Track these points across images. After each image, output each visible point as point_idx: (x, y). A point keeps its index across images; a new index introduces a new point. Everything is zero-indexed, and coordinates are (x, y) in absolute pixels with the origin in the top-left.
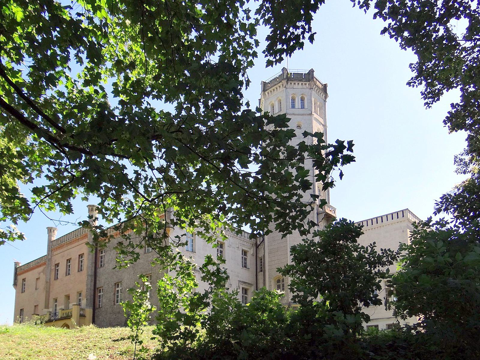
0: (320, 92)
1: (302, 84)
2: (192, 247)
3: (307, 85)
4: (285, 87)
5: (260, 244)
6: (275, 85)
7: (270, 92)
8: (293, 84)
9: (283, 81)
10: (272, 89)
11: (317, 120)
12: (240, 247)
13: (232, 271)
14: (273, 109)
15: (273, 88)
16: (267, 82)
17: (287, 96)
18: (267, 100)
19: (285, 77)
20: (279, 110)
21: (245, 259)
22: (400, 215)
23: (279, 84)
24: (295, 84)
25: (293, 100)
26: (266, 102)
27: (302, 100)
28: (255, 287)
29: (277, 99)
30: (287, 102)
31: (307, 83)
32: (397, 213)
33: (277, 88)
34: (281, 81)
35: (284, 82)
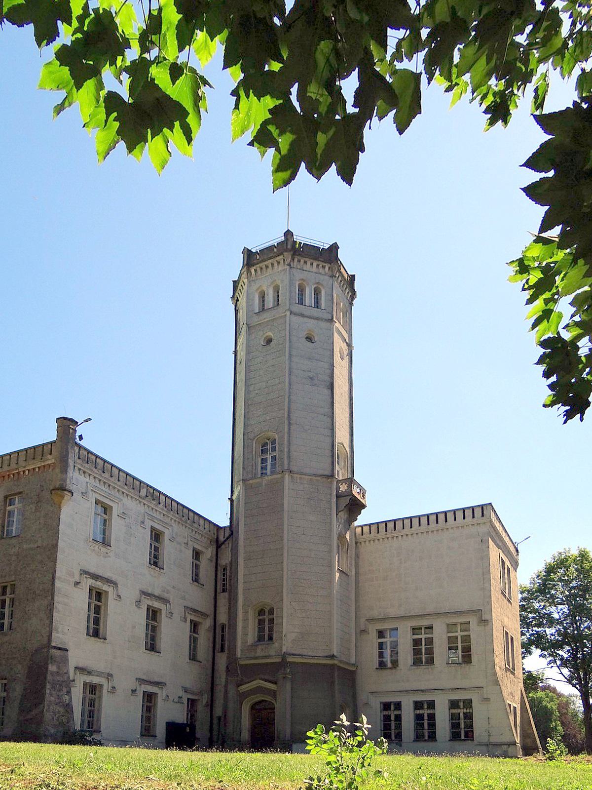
0: (345, 286)
1: (318, 265)
2: (104, 534)
3: (327, 269)
4: (289, 265)
5: (225, 541)
6: (271, 258)
7: (258, 269)
8: (302, 261)
9: (285, 254)
10: (263, 265)
11: (340, 333)
12: (190, 543)
13: (174, 587)
14: (263, 301)
15: (266, 263)
16: (254, 251)
17: (291, 281)
18: (253, 284)
19: (289, 247)
20: (274, 304)
21: (197, 567)
22: (478, 512)
23: (278, 259)
24: (305, 262)
25: (302, 290)
26: (249, 286)
27: (317, 292)
28: (212, 621)
29: (272, 283)
30: (290, 292)
31: (327, 266)
32: (473, 510)
33: (272, 265)
34: (282, 254)
35: (288, 256)
